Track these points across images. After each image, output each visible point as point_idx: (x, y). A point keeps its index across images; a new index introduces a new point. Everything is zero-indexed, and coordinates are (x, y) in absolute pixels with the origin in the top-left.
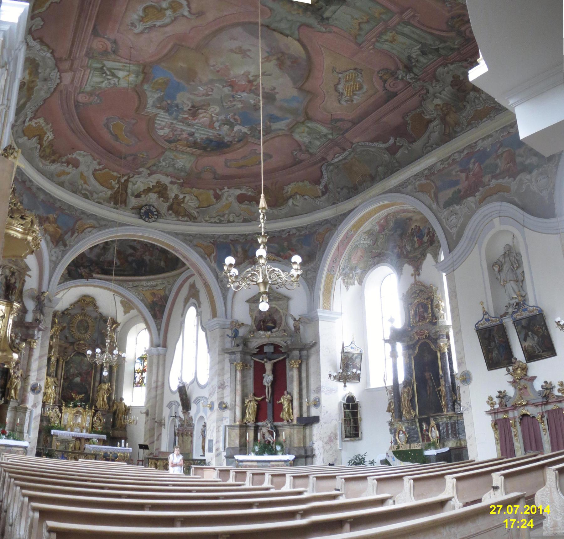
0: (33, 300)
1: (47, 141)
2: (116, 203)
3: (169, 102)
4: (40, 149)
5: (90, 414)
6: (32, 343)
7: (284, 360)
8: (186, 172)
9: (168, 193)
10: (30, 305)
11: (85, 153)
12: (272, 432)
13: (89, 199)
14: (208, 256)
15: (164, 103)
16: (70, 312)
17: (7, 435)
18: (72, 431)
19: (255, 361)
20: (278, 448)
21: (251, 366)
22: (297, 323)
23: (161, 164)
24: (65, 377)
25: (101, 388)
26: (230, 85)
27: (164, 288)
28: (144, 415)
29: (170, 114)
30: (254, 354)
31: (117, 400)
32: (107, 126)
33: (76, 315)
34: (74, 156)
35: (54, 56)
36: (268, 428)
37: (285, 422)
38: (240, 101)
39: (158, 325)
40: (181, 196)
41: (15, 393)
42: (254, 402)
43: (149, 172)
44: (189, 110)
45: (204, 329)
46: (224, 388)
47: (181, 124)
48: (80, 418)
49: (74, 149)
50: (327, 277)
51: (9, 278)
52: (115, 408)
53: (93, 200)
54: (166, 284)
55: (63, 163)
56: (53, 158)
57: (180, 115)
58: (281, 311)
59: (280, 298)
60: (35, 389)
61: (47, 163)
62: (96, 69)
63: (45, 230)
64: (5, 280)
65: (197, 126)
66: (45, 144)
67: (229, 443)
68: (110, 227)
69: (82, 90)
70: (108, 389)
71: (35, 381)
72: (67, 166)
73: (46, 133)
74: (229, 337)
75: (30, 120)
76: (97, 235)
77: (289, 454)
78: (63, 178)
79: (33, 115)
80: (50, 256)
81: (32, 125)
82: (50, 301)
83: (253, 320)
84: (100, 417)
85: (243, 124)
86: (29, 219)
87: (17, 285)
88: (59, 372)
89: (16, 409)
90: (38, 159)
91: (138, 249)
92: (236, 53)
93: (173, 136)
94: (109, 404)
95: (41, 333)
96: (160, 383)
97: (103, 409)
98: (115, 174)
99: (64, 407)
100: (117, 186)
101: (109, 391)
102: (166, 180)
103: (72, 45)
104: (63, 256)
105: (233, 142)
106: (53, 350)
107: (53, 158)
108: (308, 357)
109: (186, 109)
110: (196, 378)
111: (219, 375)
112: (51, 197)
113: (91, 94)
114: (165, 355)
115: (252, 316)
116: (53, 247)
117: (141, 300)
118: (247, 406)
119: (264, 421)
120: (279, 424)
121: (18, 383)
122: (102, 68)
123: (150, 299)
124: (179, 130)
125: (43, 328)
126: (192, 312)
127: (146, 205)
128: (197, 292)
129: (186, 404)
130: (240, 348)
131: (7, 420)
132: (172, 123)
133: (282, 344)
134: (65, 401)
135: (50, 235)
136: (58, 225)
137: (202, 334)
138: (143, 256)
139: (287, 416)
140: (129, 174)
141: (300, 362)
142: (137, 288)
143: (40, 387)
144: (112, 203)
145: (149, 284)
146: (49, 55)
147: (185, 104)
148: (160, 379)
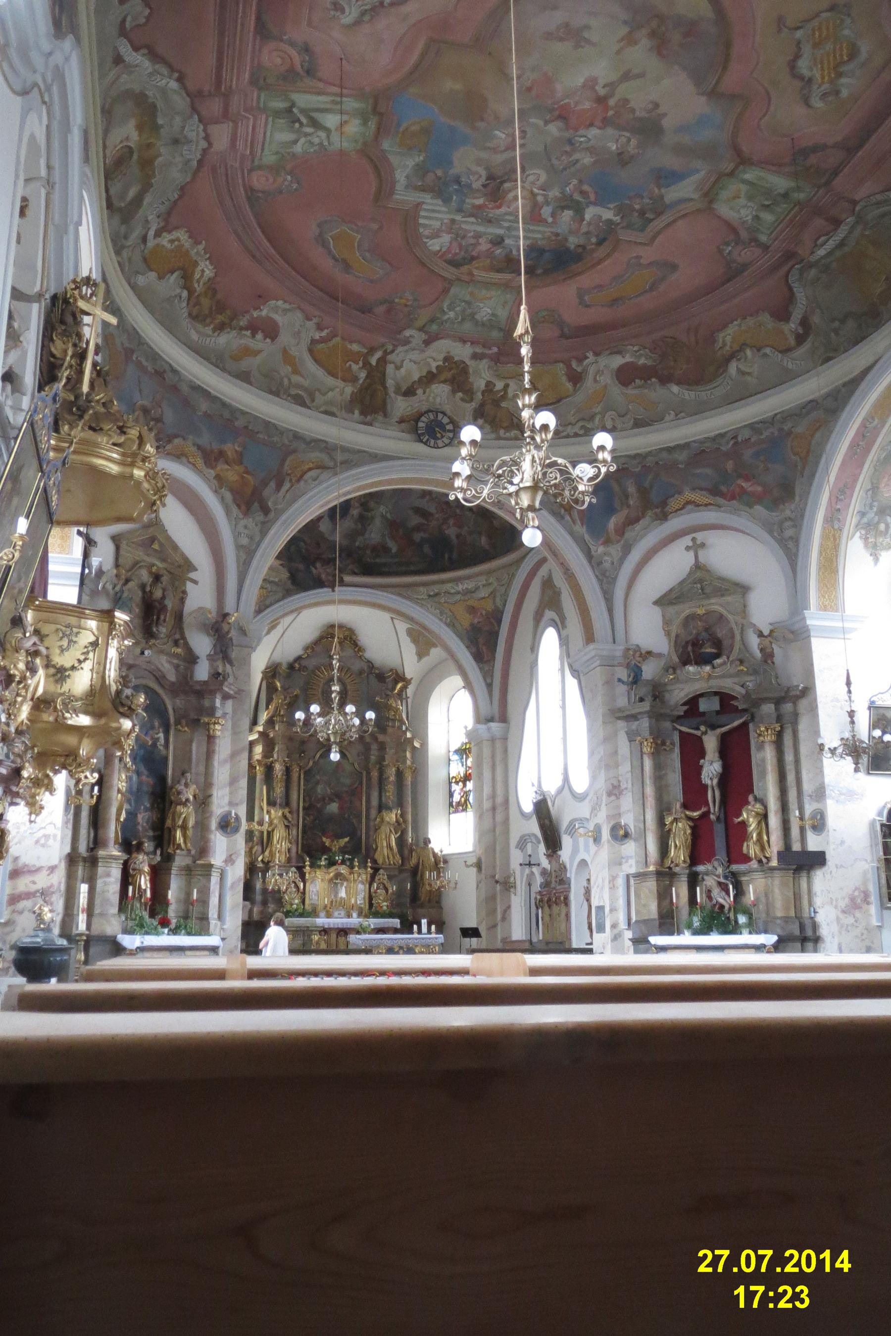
0: (208, 634)
1: (201, 283)
2: (363, 413)
3: (439, 173)
4: (189, 300)
5: (364, 877)
6: (212, 726)
7: (745, 725)
8: (501, 330)
9: (471, 380)
10: (202, 644)
11: (287, 306)
12: (727, 885)
13: (309, 408)
14: (566, 510)
15: (430, 177)
16: (304, 663)
17: (173, 926)
18: (329, 915)
19: (681, 732)
20: (742, 919)
21: (673, 744)
22: (766, 642)
23: (446, 317)
24: (307, 805)
25: (382, 820)
26: (560, 117)
27: (493, 594)
28: (474, 870)
29: (447, 201)
30: (679, 717)
31: (417, 845)
32: (321, 240)
33: (318, 668)
34: (264, 313)
35: (184, 87)
36: (718, 876)
37: (754, 864)
38: (587, 149)
39: (488, 676)
40: (499, 385)
41: (185, 836)
42: (684, 821)
43: (424, 337)
44: (484, 186)
45: (575, 673)
46: (621, 793)
47: (472, 219)
48: (344, 888)
49: (262, 297)
50: (824, 537)
51: (148, 589)
52: (414, 861)
53: (317, 409)
54: (495, 584)
55: (241, 329)
56: (220, 318)
57: (467, 200)
58: (730, 617)
59: (727, 590)
60: (226, 825)
61: (209, 330)
62: (277, 114)
63: (218, 477)
64: (140, 593)
65: (506, 221)
66: (199, 288)
67: (637, 912)
68: (357, 465)
69: (256, 163)
70: (397, 821)
71: (227, 809)
72: (253, 336)
73: (196, 264)
74: (623, 682)
75: (158, 234)
77: (766, 932)
78: (251, 363)
79: (162, 224)
80: (236, 535)
81: (163, 246)
82: (243, 632)
83: (672, 644)
84: (385, 882)
85: (600, 202)
86: (134, 433)
87: (169, 604)
88: (294, 796)
89: (188, 871)
90: (185, 323)
91: (431, 515)
92: (561, 40)
93: (460, 249)
94: (402, 856)
95: (229, 703)
96: (499, 800)
97: (390, 864)
98: (355, 347)
99: (308, 868)
100: (363, 375)
101: (400, 826)
102: (462, 352)
103: (220, 60)
104: (264, 533)
105: (588, 248)
106: (276, 749)
107: (220, 318)
108: (796, 715)
109: (477, 185)
110: (566, 779)
111: (608, 767)
112: (224, 404)
113: (275, 170)
114: (505, 739)
115: (668, 634)
116: (241, 516)
117: (448, 625)
118: (670, 830)
119: (709, 861)
120: (742, 867)
121: (188, 814)
122: (289, 110)
123: (466, 620)
124: (472, 234)
125: (232, 692)
126: (550, 639)
127: (429, 411)
128: (557, 594)
129: (552, 840)
130: (646, 706)
131: (170, 896)
132: (453, 221)
133: (738, 691)
134: (311, 857)
135: (232, 490)
136: (246, 467)
137: (572, 683)
138: (444, 527)
139: (757, 849)
140: (383, 345)
141: (778, 729)
142: (436, 599)
143: (237, 818)
144: (357, 412)
145: (460, 587)
146: (174, 85)
147: (474, 173)
148: (500, 791)
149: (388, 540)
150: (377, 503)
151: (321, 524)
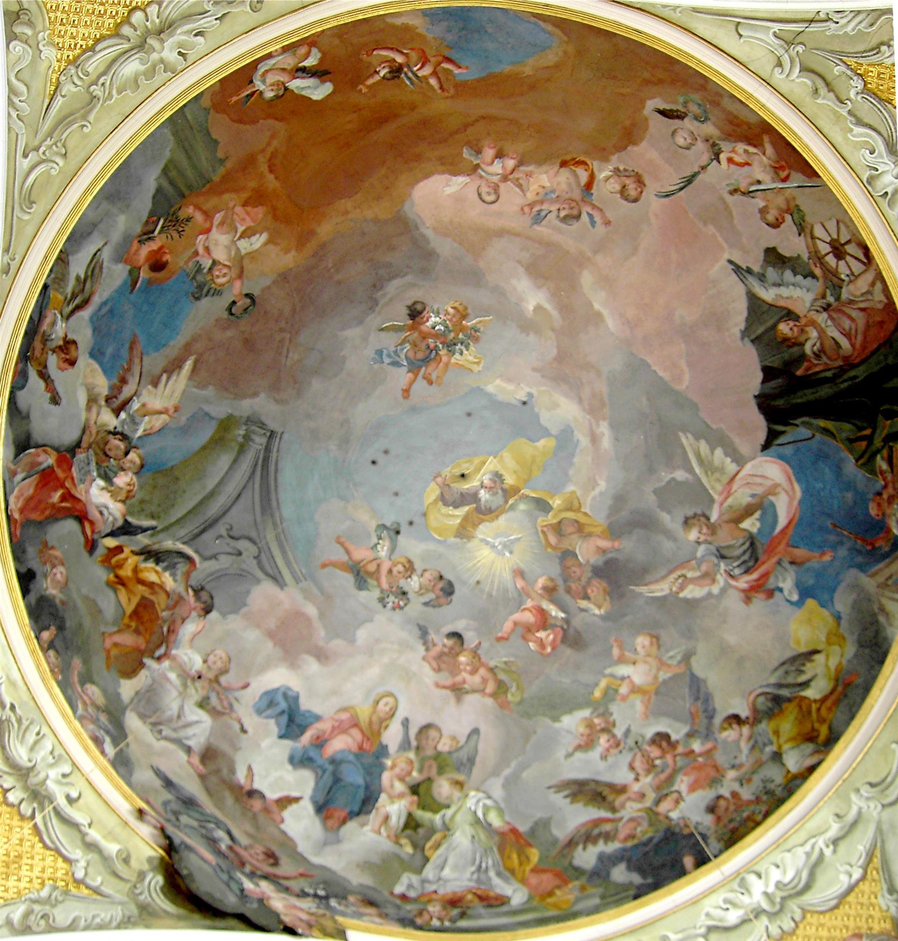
76: (276, 479)
91: (622, 790)
109: (598, 530)
149: (496, 881)
150: (460, 785)
151: (287, 814)
